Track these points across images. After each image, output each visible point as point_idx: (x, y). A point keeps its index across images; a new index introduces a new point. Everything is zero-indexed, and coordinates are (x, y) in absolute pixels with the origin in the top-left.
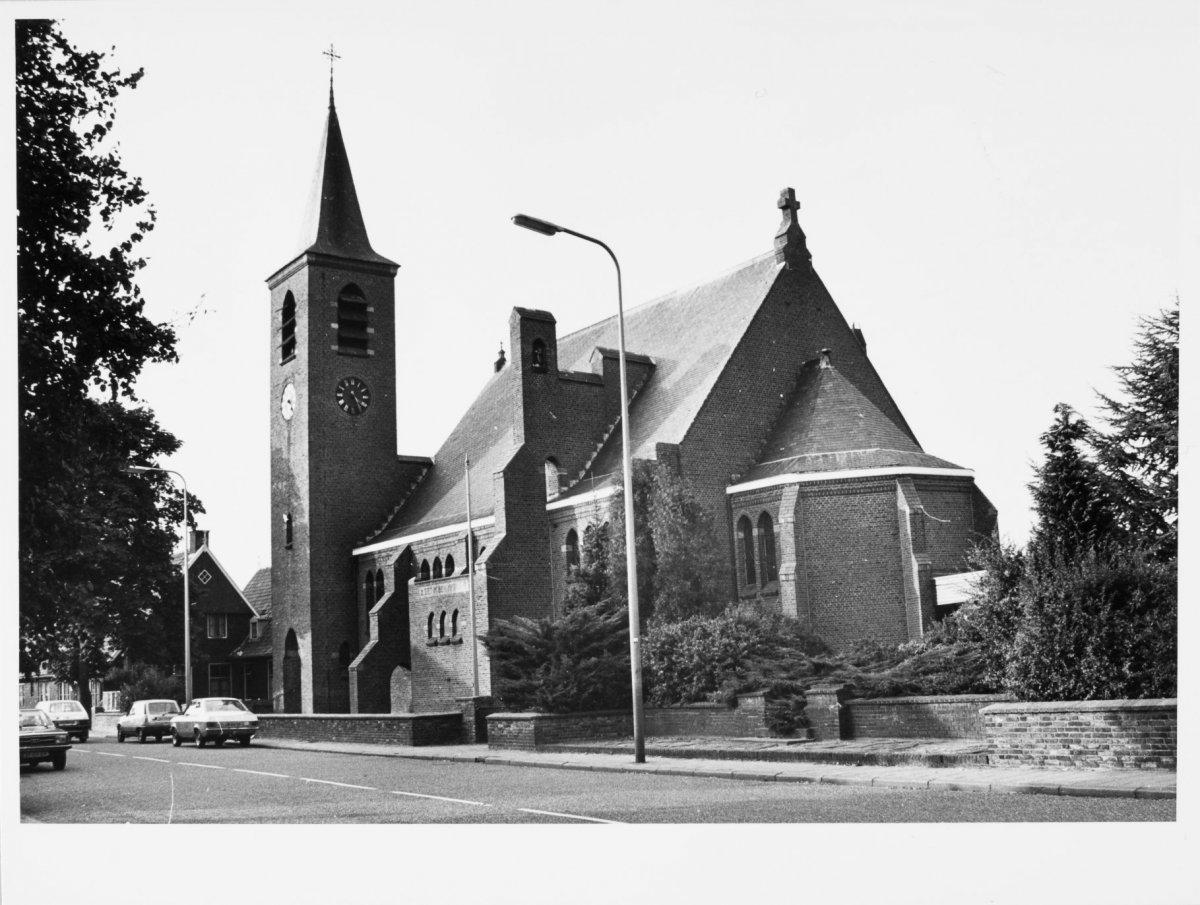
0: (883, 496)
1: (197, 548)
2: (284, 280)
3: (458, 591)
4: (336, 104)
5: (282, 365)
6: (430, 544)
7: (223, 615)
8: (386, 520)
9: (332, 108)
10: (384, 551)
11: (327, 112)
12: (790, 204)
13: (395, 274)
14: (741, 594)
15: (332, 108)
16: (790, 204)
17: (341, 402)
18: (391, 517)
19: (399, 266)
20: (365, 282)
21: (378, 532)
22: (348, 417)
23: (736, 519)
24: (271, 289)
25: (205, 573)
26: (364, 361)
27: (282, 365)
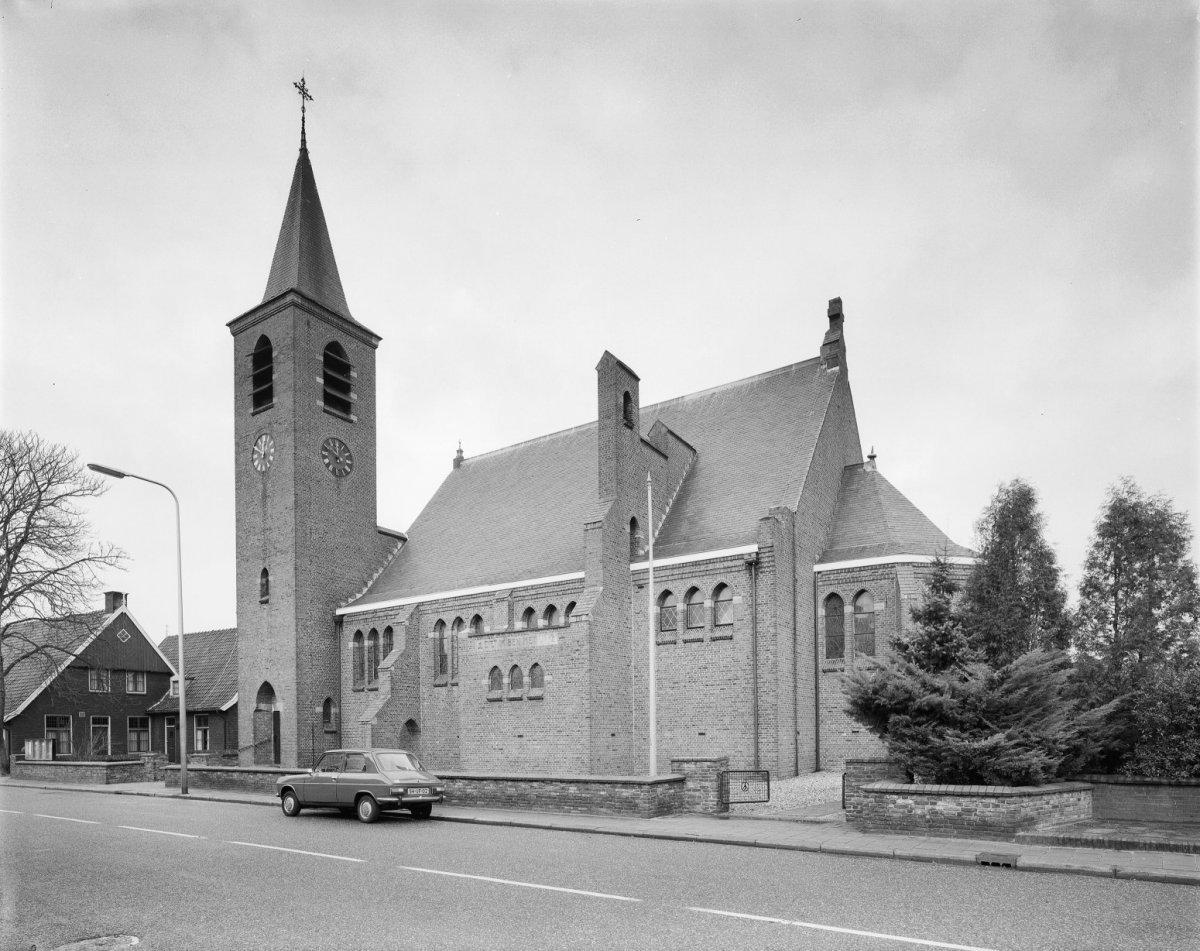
0: (198, 707)
1: (115, 608)
2: (254, 324)
3: (539, 644)
4: (308, 146)
5: (253, 415)
6: (450, 604)
7: (142, 672)
8: (366, 584)
9: (304, 151)
10: (381, 610)
11: (297, 155)
12: (836, 315)
13: (375, 347)
14: (334, 729)
15: (304, 151)
16: (836, 315)
17: (327, 461)
18: (370, 583)
19: (380, 339)
20: (350, 347)
21: (359, 596)
22: (333, 478)
23: (821, 597)
24: (234, 334)
25: (123, 633)
26: (347, 424)
27: (253, 415)
